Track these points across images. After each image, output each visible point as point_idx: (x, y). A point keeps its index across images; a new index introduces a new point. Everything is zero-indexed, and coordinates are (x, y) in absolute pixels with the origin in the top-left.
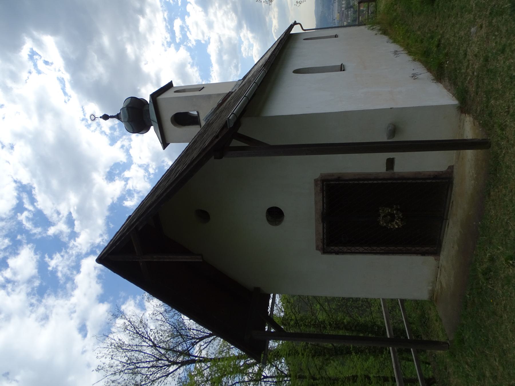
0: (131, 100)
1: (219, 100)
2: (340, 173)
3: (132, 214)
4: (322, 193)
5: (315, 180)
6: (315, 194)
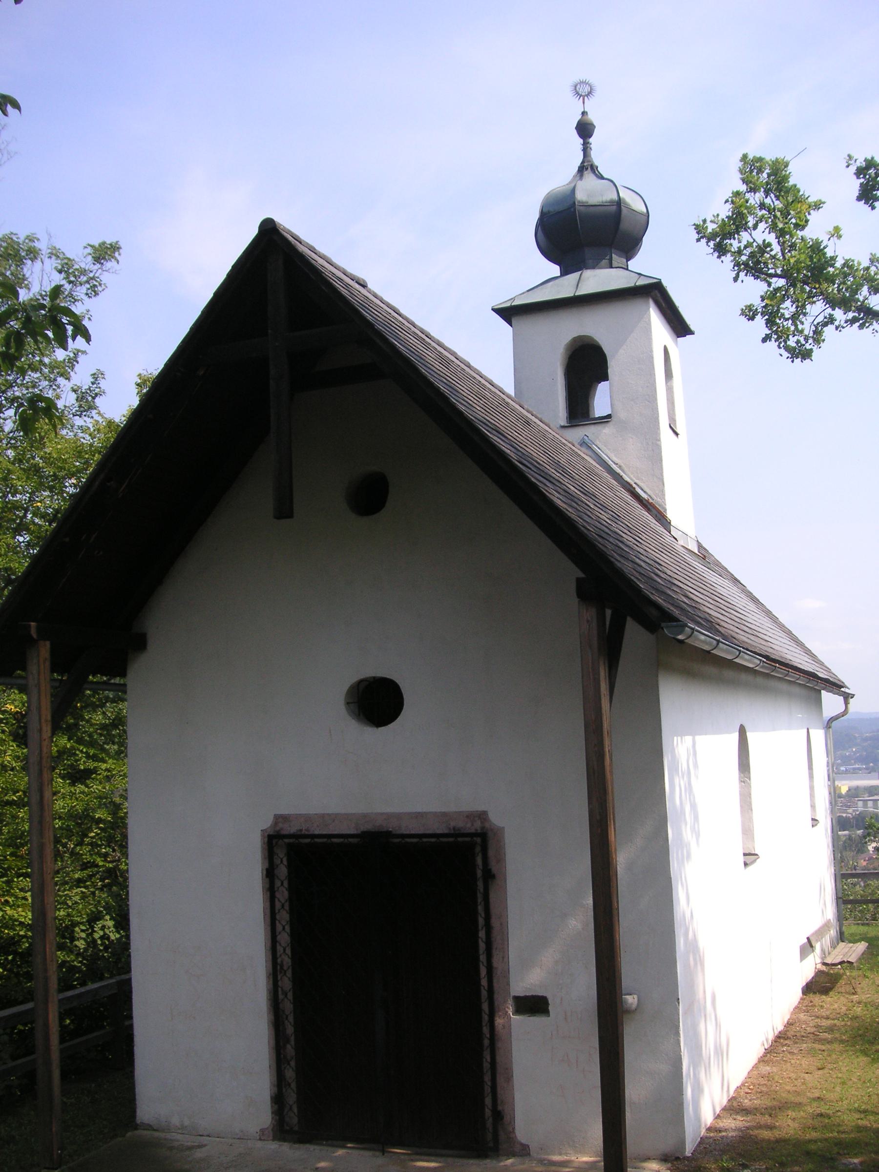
0: (641, 214)
3: (370, 291)
4: (446, 831)
5: (484, 813)
6: (444, 814)
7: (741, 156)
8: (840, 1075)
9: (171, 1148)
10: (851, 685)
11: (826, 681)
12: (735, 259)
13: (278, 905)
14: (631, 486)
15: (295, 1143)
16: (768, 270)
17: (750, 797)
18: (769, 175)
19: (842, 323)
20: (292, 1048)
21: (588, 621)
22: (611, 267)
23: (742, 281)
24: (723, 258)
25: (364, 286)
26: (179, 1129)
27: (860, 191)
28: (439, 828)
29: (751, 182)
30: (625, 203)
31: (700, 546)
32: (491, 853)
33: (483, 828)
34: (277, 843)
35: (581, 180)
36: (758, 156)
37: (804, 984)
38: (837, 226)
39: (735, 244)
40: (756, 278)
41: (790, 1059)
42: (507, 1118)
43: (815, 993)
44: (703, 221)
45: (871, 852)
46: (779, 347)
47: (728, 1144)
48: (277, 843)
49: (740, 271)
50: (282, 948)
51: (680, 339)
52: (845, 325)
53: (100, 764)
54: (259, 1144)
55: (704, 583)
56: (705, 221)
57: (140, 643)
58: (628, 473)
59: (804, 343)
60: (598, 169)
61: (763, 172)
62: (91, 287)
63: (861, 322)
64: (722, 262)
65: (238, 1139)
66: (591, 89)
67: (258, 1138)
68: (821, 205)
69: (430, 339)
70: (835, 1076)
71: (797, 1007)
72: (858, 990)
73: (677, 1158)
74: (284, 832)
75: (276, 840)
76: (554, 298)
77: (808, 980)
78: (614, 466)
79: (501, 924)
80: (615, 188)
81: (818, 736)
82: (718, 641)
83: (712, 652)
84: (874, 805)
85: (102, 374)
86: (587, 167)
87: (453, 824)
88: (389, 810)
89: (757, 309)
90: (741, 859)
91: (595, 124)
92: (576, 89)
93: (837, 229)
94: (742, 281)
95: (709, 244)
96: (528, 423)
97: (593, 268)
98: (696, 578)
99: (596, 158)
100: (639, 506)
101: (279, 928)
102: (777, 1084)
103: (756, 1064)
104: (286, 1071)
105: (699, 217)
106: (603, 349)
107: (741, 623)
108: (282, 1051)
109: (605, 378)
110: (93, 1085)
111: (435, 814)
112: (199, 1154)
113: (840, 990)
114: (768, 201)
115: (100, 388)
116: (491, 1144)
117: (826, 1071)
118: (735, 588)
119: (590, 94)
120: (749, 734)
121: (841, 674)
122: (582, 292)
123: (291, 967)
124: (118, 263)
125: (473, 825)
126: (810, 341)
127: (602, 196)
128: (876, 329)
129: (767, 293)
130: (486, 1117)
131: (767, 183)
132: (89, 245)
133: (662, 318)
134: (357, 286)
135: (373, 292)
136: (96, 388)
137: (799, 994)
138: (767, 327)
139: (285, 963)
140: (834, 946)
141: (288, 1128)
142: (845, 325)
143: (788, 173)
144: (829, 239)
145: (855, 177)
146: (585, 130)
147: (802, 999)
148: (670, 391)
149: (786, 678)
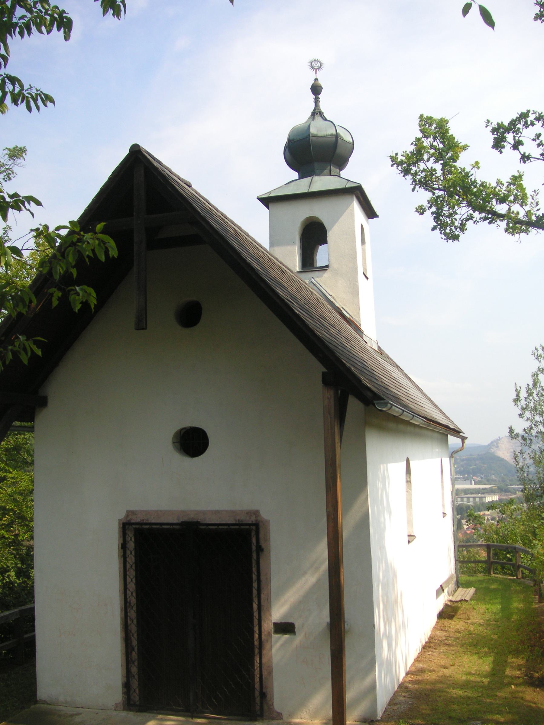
1: (349, 311)
2: (270, 550)
3: (193, 189)
4: (234, 522)
6: (233, 512)
7: (419, 116)
8: (464, 670)
9: (60, 716)
10: (466, 432)
11: (454, 430)
12: (413, 178)
13: (128, 566)
14: (340, 309)
15: (137, 712)
16: (433, 185)
17: (411, 501)
18: (436, 128)
19: (478, 220)
20: (136, 653)
21: (328, 398)
22: (331, 175)
23: (417, 191)
24: (406, 177)
25: (190, 186)
26: (64, 703)
27: (494, 142)
28: (231, 521)
29: (426, 132)
30: (340, 136)
31: (379, 347)
32: (261, 536)
33: (257, 520)
34: (128, 528)
35: (313, 121)
36: (429, 116)
37: (438, 613)
38: (477, 161)
39: (414, 169)
40: (426, 189)
41: (434, 659)
42: (268, 697)
43: (445, 618)
44: (395, 154)
45: (465, 529)
46: (441, 234)
47: (402, 712)
48: (128, 528)
49: (416, 185)
50: (131, 593)
51: (370, 220)
52: (479, 221)
53: (7, 474)
54: (115, 713)
55: (385, 371)
56: (397, 154)
57: (43, 402)
58: (338, 301)
59: (454, 230)
60: (324, 114)
61: (432, 126)
62: (7, 174)
63: (490, 220)
64: (406, 179)
65: (101, 709)
66: (321, 65)
67: (114, 709)
68: (467, 148)
69: (226, 219)
70: (461, 670)
71: (434, 628)
72: (471, 617)
73: (372, 721)
74: (133, 521)
75: (128, 526)
76: (295, 193)
77: (440, 610)
78: (329, 297)
79: (267, 579)
80: (334, 127)
81: (446, 461)
82: (403, 411)
83: (399, 417)
84: (473, 500)
85: (10, 228)
86: (317, 113)
87: (238, 518)
88: (199, 508)
89: (425, 208)
90: (406, 539)
91: (322, 87)
92: (311, 65)
93: (477, 163)
94: (417, 191)
95: (398, 168)
96: (283, 271)
97: (319, 175)
98: (381, 368)
99: (323, 107)
100: (345, 322)
101: (129, 580)
102: (427, 675)
103: (413, 663)
104: (132, 668)
105: (393, 151)
106: (325, 225)
107: (408, 395)
108: (129, 656)
109: (325, 242)
110: (6, 675)
111: (227, 511)
112: (77, 719)
113: (459, 617)
114: (435, 144)
115: (8, 237)
116: (259, 713)
117: (456, 667)
118: (399, 372)
119: (320, 67)
120: (411, 462)
121: (460, 424)
122: (312, 190)
123: (135, 605)
124: (25, 160)
125: (250, 518)
126: (458, 229)
127: (326, 131)
128: (499, 224)
129: (431, 198)
130: (256, 697)
131: (435, 133)
132: (7, 148)
133: (360, 206)
134: (187, 187)
135: (195, 190)
136: (6, 237)
137: (435, 619)
138: (434, 221)
139: (132, 602)
140: (455, 591)
141: (133, 703)
142: (479, 221)
143: (448, 127)
144: (472, 169)
145: (491, 133)
146: (316, 90)
147: (437, 622)
148: (364, 251)
149: (435, 430)
